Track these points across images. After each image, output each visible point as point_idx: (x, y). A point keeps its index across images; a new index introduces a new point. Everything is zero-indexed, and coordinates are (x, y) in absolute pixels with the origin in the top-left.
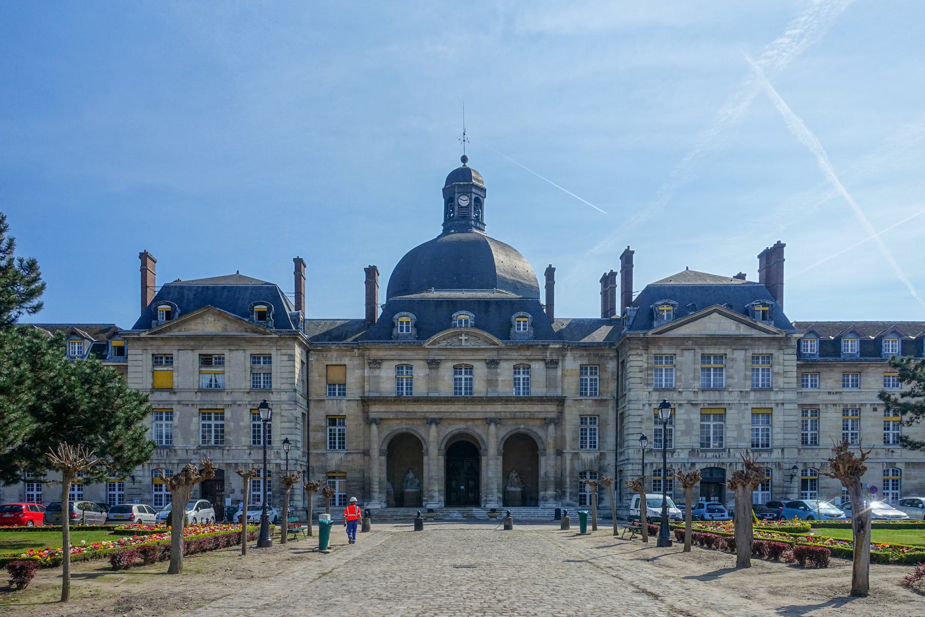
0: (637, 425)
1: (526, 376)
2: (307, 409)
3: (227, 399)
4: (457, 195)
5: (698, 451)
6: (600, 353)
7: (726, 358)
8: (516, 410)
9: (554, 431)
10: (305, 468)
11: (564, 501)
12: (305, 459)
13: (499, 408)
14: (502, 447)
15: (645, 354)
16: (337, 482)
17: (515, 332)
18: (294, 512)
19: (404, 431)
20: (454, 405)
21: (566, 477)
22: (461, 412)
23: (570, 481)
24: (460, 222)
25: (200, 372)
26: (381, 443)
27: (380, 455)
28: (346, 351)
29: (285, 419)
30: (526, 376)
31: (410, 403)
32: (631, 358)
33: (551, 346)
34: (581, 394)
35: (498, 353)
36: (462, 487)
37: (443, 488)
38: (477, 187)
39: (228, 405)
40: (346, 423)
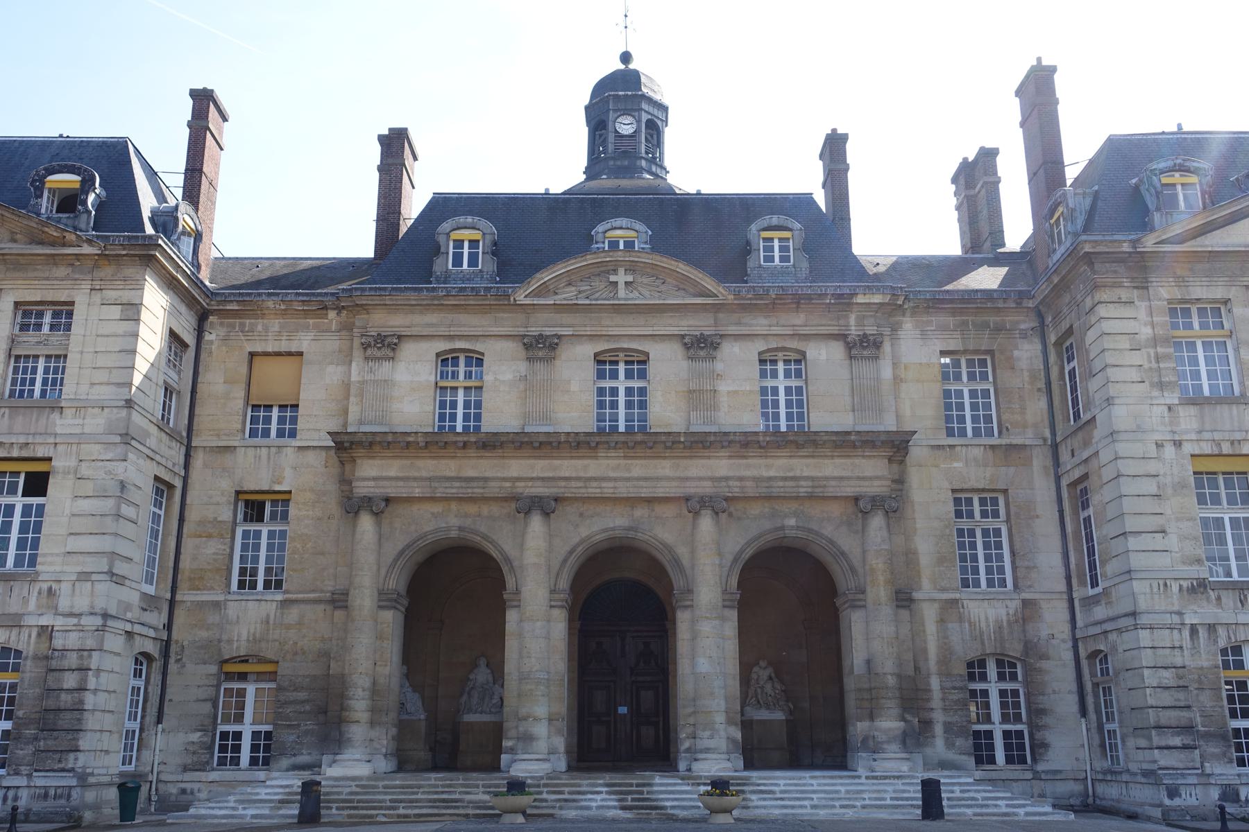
0: (1149, 505)
1: (794, 383)
4: (612, 115)
6: (993, 319)
8: (772, 473)
9: (885, 534)
11: (928, 751)
12: (158, 619)
13: (721, 466)
14: (734, 582)
15: (1141, 298)
16: (251, 689)
17: (760, 266)
18: (74, 794)
19: (454, 534)
20: (596, 458)
21: (929, 675)
22: (615, 479)
23: (942, 688)
24: (619, 163)
26: (383, 571)
28: (306, 314)
29: (88, 488)
30: (794, 383)
31: (472, 452)
32: (1102, 311)
33: (860, 299)
34: (950, 432)
35: (716, 320)
36: (623, 710)
37: (562, 708)
38: (650, 101)
40: (293, 511)
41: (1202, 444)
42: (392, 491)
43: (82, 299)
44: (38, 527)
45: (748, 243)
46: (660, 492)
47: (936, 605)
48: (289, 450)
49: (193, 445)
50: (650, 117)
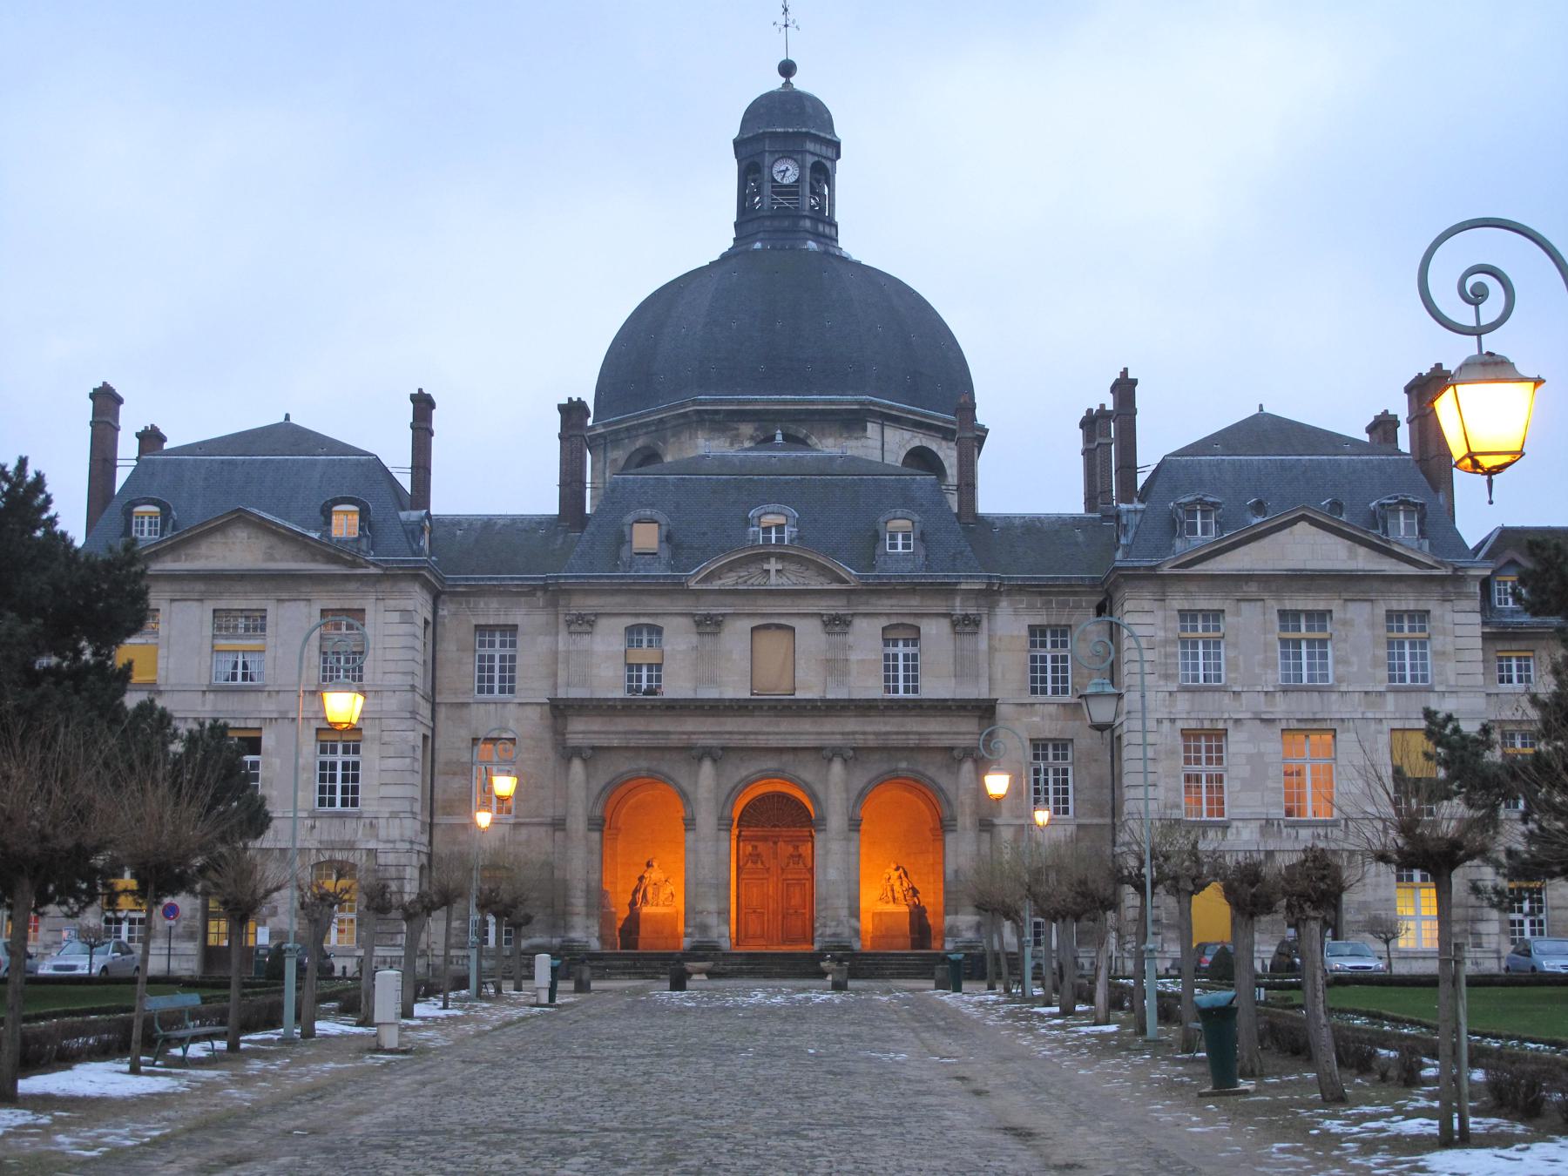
2: (431, 725)
3: (268, 706)
4: (768, 159)
5: (1279, 825)
7: (1331, 618)
10: (424, 859)
12: (425, 838)
13: (852, 724)
17: (886, 553)
20: (753, 716)
22: (768, 733)
25: (213, 647)
26: (591, 804)
27: (589, 830)
29: (391, 751)
34: (1034, 691)
39: (271, 719)
41: (1190, 721)
42: (596, 743)
43: (369, 605)
44: (356, 778)
45: (877, 532)
46: (802, 744)
47: (1012, 829)
48: (511, 707)
49: (437, 701)
50: (816, 159)
